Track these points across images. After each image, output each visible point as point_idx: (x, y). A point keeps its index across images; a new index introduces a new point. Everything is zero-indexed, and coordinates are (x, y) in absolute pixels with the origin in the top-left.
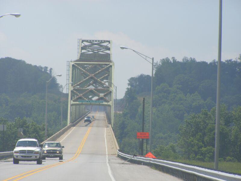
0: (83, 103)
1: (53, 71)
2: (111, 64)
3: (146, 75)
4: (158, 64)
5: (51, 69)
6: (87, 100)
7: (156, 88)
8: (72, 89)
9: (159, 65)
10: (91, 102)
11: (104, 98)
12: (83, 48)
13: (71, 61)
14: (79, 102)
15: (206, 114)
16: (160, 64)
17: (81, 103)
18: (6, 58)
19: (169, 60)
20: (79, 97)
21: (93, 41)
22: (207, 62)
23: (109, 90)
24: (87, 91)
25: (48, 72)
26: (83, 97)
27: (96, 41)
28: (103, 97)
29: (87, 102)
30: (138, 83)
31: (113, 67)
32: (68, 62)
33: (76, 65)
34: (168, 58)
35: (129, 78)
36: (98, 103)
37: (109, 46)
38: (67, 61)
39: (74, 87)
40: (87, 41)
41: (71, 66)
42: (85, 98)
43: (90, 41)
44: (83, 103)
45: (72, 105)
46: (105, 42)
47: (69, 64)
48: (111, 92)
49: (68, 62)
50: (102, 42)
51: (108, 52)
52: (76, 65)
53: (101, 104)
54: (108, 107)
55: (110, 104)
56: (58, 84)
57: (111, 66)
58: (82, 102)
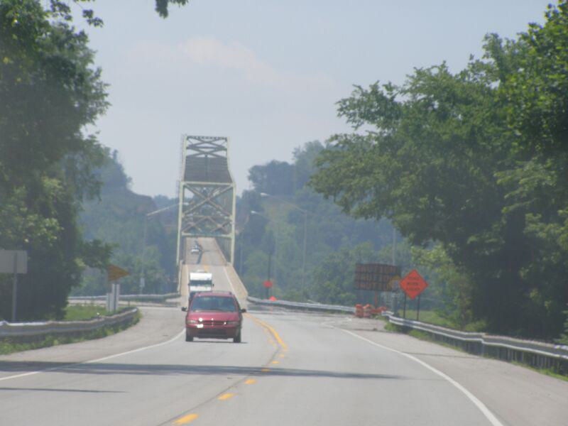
1: (118, 155)
2: (232, 185)
5: (116, 151)
12: (189, 147)
15: (346, 254)
16: (305, 150)
21: (203, 138)
25: (111, 157)
27: (207, 138)
30: (265, 177)
31: (234, 190)
35: (250, 166)
37: (225, 145)
39: (186, 214)
40: (195, 138)
43: (199, 137)
46: (219, 139)
50: (216, 139)
51: (221, 153)
54: (226, 241)
56: (125, 176)
57: (232, 188)
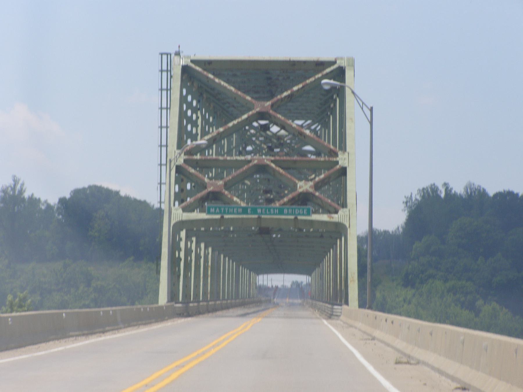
0: (226, 216)
3: (382, 230)
4: (414, 199)
6: (243, 205)
7: (414, 246)
8: (181, 161)
9: (416, 199)
10: (259, 211)
11: (313, 195)
13: (178, 54)
14: (209, 213)
17: (218, 217)
18: (90, 187)
19: (437, 188)
20: (209, 193)
22: (515, 192)
23: (337, 163)
24: (245, 168)
26: (226, 192)
28: (311, 190)
29: (245, 211)
32: (165, 57)
33: (198, 68)
34: (434, 184)
36: (292, 217)
38: (162, 54)
41: (177, 72)
42: (235, 199)
44: (226, 216)
45: (180, 225)
47: (170, 63)
48: (343, 171)
49: (165, 57)
52: (198, 68)
53: (305, 221)
55: (341, 220)
58: (220, 213)
